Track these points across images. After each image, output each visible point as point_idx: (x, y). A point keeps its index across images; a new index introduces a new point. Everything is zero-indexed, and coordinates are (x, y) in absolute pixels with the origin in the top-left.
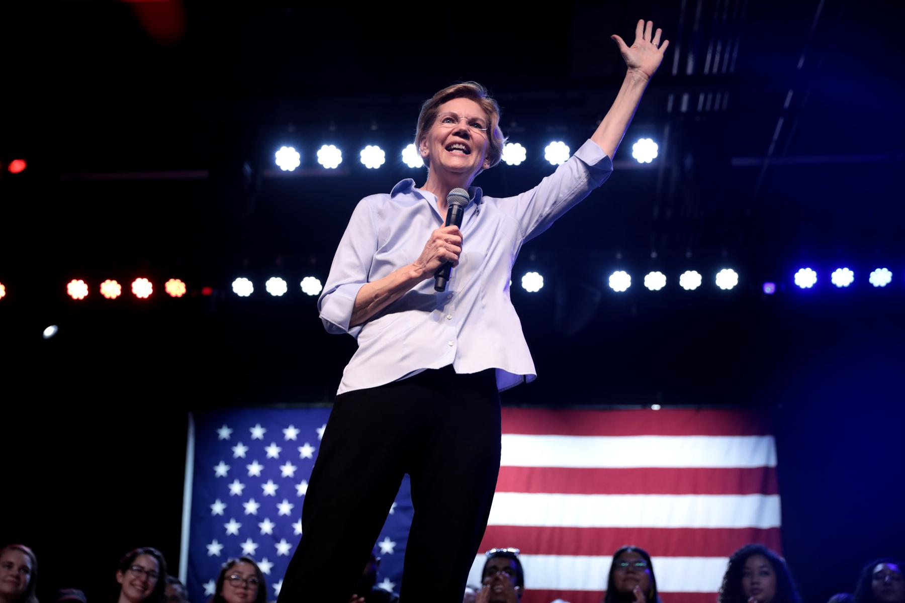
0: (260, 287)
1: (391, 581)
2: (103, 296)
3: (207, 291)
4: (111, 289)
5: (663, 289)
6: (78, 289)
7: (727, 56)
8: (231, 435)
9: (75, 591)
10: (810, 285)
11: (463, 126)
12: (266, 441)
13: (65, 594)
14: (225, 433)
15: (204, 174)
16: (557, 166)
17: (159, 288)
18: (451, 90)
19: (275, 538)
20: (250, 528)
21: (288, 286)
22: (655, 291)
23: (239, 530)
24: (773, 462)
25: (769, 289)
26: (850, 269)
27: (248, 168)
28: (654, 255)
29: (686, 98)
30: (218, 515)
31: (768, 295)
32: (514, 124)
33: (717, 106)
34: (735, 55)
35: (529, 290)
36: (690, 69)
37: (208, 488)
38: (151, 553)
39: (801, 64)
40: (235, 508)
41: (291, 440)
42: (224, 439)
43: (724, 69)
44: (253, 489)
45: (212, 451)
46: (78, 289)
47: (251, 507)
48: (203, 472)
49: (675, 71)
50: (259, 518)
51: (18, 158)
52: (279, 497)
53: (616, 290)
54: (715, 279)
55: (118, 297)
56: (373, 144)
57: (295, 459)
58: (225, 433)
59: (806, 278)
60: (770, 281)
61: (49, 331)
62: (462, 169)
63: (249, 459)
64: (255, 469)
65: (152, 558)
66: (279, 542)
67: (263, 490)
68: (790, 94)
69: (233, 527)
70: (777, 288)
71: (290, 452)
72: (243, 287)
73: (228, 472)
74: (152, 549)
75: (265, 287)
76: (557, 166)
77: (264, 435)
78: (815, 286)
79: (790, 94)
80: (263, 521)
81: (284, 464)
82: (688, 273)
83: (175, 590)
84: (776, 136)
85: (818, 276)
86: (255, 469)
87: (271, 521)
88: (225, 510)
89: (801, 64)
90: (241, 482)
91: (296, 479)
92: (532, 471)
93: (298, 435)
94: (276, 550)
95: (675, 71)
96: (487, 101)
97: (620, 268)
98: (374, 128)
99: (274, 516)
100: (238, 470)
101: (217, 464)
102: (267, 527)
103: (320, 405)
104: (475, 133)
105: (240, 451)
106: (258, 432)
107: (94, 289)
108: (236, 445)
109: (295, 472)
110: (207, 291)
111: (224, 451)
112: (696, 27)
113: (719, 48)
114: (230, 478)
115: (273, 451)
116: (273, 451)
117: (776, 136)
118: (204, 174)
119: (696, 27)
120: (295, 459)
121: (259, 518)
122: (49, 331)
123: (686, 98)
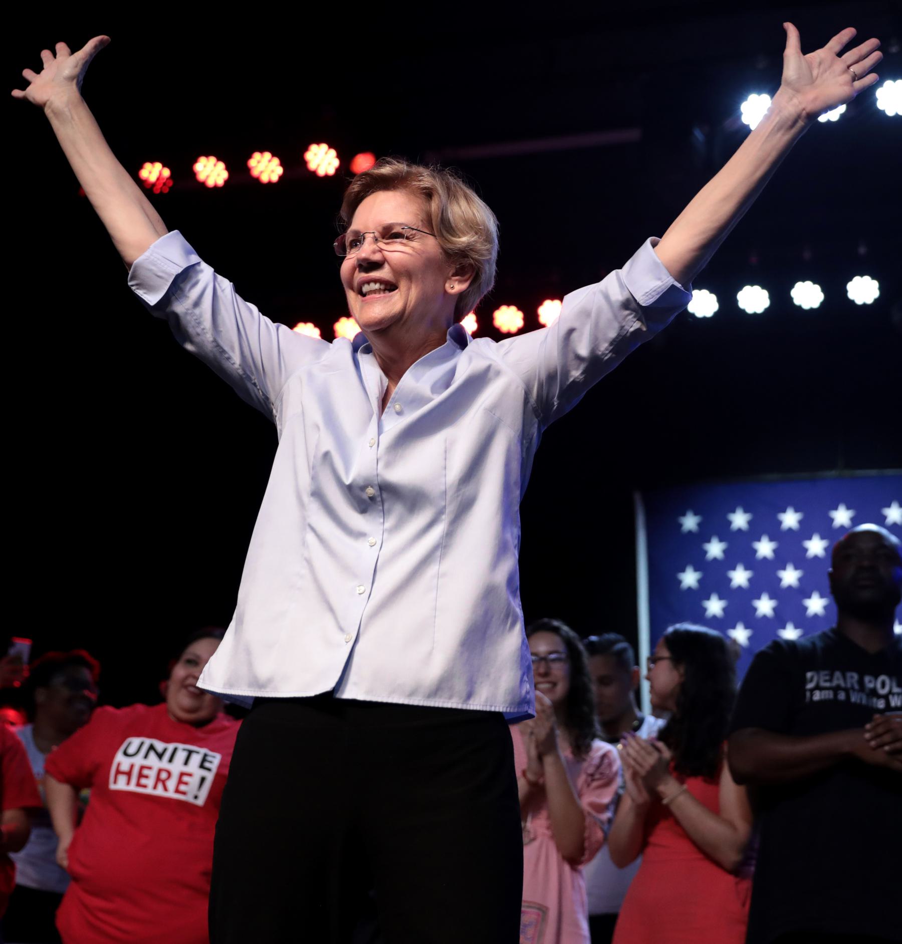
8: (700, 525)
11: (366, 250)
12: (754, 533)
14: (690, 522)
15: (633, 135)
16: (543, 326)
27: (699, 135)
38: (556, 630)
41: (790, 530)
45: (674, 551)
48: (664, 583)
57: (800, 560)
63: (730, 561)
65: (556, 639)
67: (755, 609)
71: (790, 548)
73: (700, 581)
74: (556, 623)
75: (823, 290)
76: (543, 326)
81: (784, 569)
90: (721, 598)
91: (803, 591)
93: (800, 522)
96: (426, 178)
100: (715, 579)
101: (683, 570)
103: (833, 473)
104: (398, 253)
105: (715, 549)
106: (790, 519)
109: (800, 580)
111: (690, 550)
115: (765, 548)
118: (633, 135)
120: (800, 560)
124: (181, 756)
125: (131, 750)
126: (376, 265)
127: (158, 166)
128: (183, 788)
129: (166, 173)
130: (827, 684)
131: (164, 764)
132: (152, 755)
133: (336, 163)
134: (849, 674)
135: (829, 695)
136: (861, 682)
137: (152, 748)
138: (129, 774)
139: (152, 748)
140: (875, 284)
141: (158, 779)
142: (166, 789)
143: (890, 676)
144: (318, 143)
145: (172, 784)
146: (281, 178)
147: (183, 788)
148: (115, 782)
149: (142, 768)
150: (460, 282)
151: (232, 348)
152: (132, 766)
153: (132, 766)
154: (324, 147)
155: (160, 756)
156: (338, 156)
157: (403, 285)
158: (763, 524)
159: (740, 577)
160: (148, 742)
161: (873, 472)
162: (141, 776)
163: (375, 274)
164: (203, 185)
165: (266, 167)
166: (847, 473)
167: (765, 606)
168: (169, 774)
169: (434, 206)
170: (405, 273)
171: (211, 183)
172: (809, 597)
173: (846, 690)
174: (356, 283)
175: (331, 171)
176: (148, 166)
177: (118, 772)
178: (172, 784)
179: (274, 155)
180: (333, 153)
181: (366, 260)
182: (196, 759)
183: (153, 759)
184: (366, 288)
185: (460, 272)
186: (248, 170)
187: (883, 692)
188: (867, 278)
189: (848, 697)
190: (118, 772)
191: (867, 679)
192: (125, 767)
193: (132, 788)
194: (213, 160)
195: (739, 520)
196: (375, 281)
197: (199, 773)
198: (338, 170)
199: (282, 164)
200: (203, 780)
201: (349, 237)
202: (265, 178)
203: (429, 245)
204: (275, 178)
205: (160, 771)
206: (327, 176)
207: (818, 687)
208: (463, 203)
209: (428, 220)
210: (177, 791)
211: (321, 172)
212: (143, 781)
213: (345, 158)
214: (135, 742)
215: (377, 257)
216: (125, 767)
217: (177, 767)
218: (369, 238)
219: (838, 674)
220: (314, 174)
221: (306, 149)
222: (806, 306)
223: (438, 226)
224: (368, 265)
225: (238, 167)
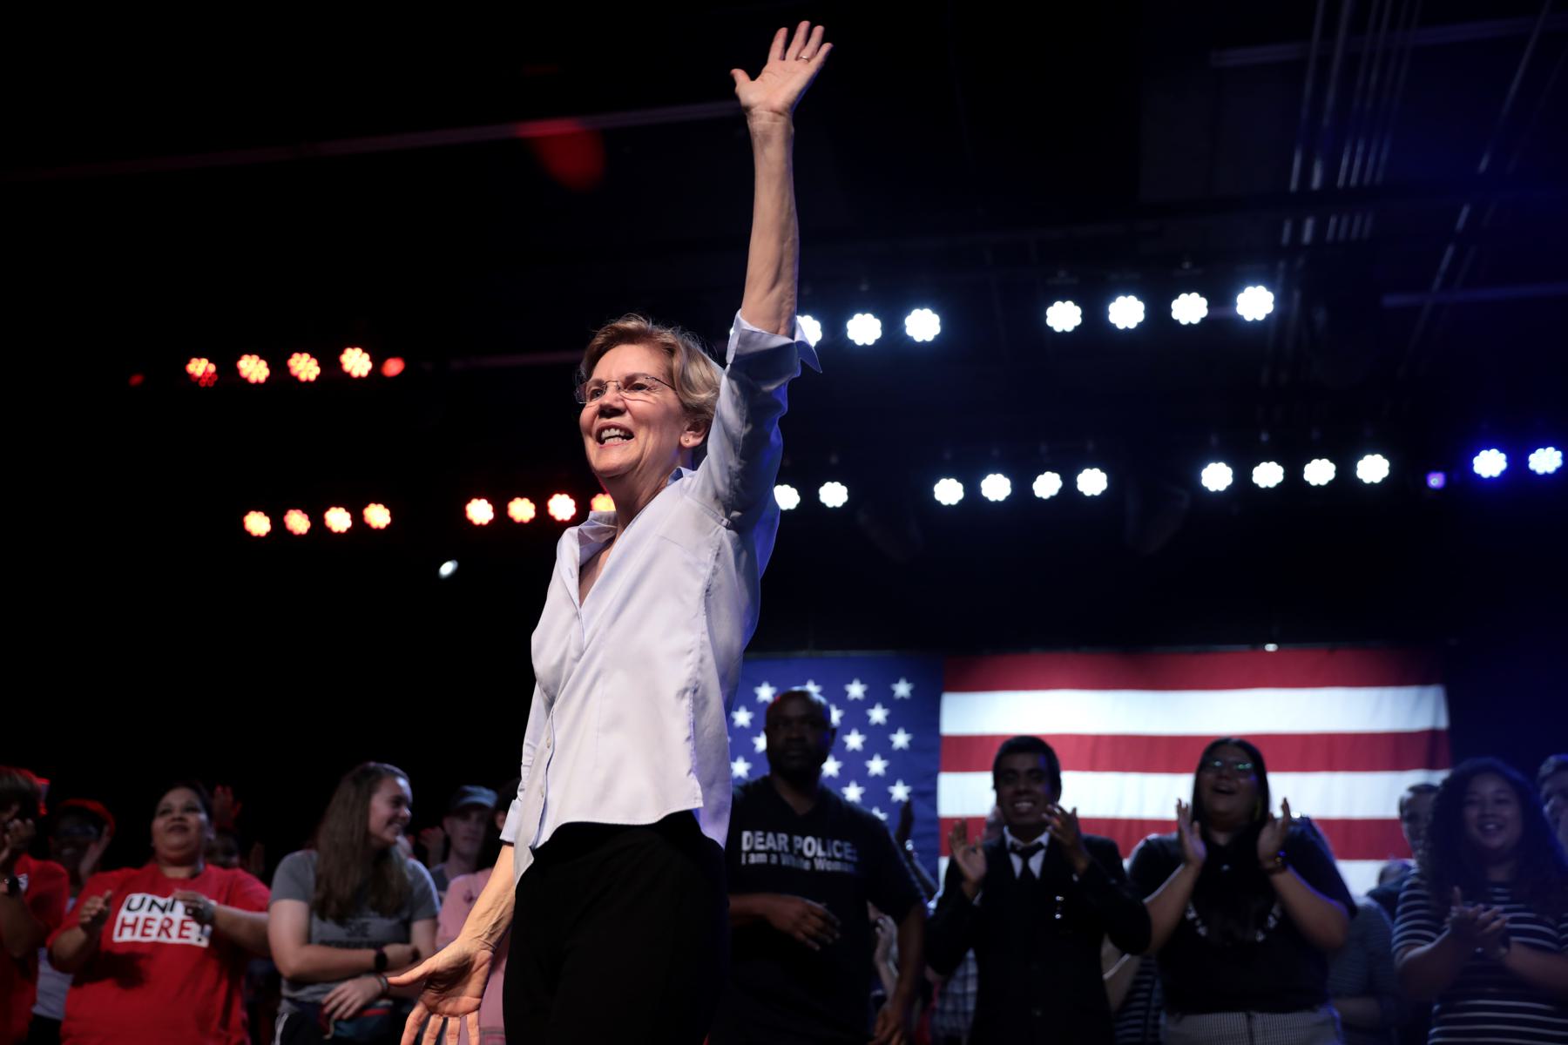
0: (972, 490)
5: (961, 502)
6: (480, 511)
7: (1371, 160)
10: (954, 502)
11: (609, 397)
18: (599, 340)
21: (818, 495)
24: (1443, 723)
25: (1435, 481)
26: (1501, 451)
28: (1264, 437)
29: (1309, 224)
31: (1435, 490)
32: (1062, 274)
33: (1354, 234)
34: (1384, 157)
35: (830, 505)
36: (1316, 182)
39: (1483, 165)
43: (1367, 180)
46: (480, 511)
49: (1294, 185)
51: (393, 355)
52: (867, 753)
53: (945, 502)
54: (1200, 478)
56: (864, 312)
58: (902, 689)
59: (1490, 463)
60: (1436, 470)
61: (447, 569)
62: (617, 469)
68: (1465, 211)
70: (1448, 480)
78: (1504, 474)
79: (1465, 211)
82: (1368, 458)
84: (1444, 265)
85: (980, 489)
89: (1483, 165)
92: (1098, 741)
95: (1294, 185)
96: (668, 336)
97: (1217, 459)
98: (864, 288)
99: (862, 778)
103: (803, 653)
104: (638, 402)
107: (972, 490)
112: (1326, 122)
113: (1360, 149)
117: (1444, 265)
119: (1326, 122)
122: (447, 569)
123: (1309, 224)
125: (135, 905)
126: (618, 412)
127: (204, 362)
128: (185, 933)
129: (212, 368)
130: (761, 847)
132: (155, 908)
133: (369, 366)
134: (780, 836)
135: (762, 858)
136: (791, 844)
137: (153, 903)
138: (134, 926)
139: (153, 903)
140: (844, 490)
142: (169, 936)
143: (816, 837)
144: (353, 347)
145: (174, 931)
147: (185, 933)
148: (120, 934)
149: (147, 919)
155: (163, 910)
156: (371, 360)
157: (641, 434)
160: (149, 898)
161: (838, 653)
162: (145, 926)
163: (615, 420)
164: (246, 380)
165: (305, 367)
167: (878, 715)
168: (171, 922)
169: (676, 363)
170: (643, 421)
171: (253, 379)
173: (778, 853)
174: (595, 430)
175: (364, 373)
176: (194, 361)
177: (123, 925)
178: (174, 931)
181: (609, 406)
183: (156, 912)
184: (606, 434)
186: (288, 369)
187: (809, 854)
189: (779, 860)
191: (797, 838)
193: (137, 937)
194: (255, 358)
195: (856, 690)
196: (616, 427)
199: (319, 365)
201: (591, 386)
202: (303, 377)
204: (312, 377)
206: (360, 378)
207: (753, 851)
208: (702, 365)
209: (670, 374)
210: (180, 936)
211: (355, 374)
212: (148, 931)
213: (378, 361)
214: (136, 899)
215: (619, 405)
218: (612, 387)
219: (770, 836)
220: (348, 375)
221: (342, 352)
223: (676, 381)
224: (607, 412)
225: (330, 363)
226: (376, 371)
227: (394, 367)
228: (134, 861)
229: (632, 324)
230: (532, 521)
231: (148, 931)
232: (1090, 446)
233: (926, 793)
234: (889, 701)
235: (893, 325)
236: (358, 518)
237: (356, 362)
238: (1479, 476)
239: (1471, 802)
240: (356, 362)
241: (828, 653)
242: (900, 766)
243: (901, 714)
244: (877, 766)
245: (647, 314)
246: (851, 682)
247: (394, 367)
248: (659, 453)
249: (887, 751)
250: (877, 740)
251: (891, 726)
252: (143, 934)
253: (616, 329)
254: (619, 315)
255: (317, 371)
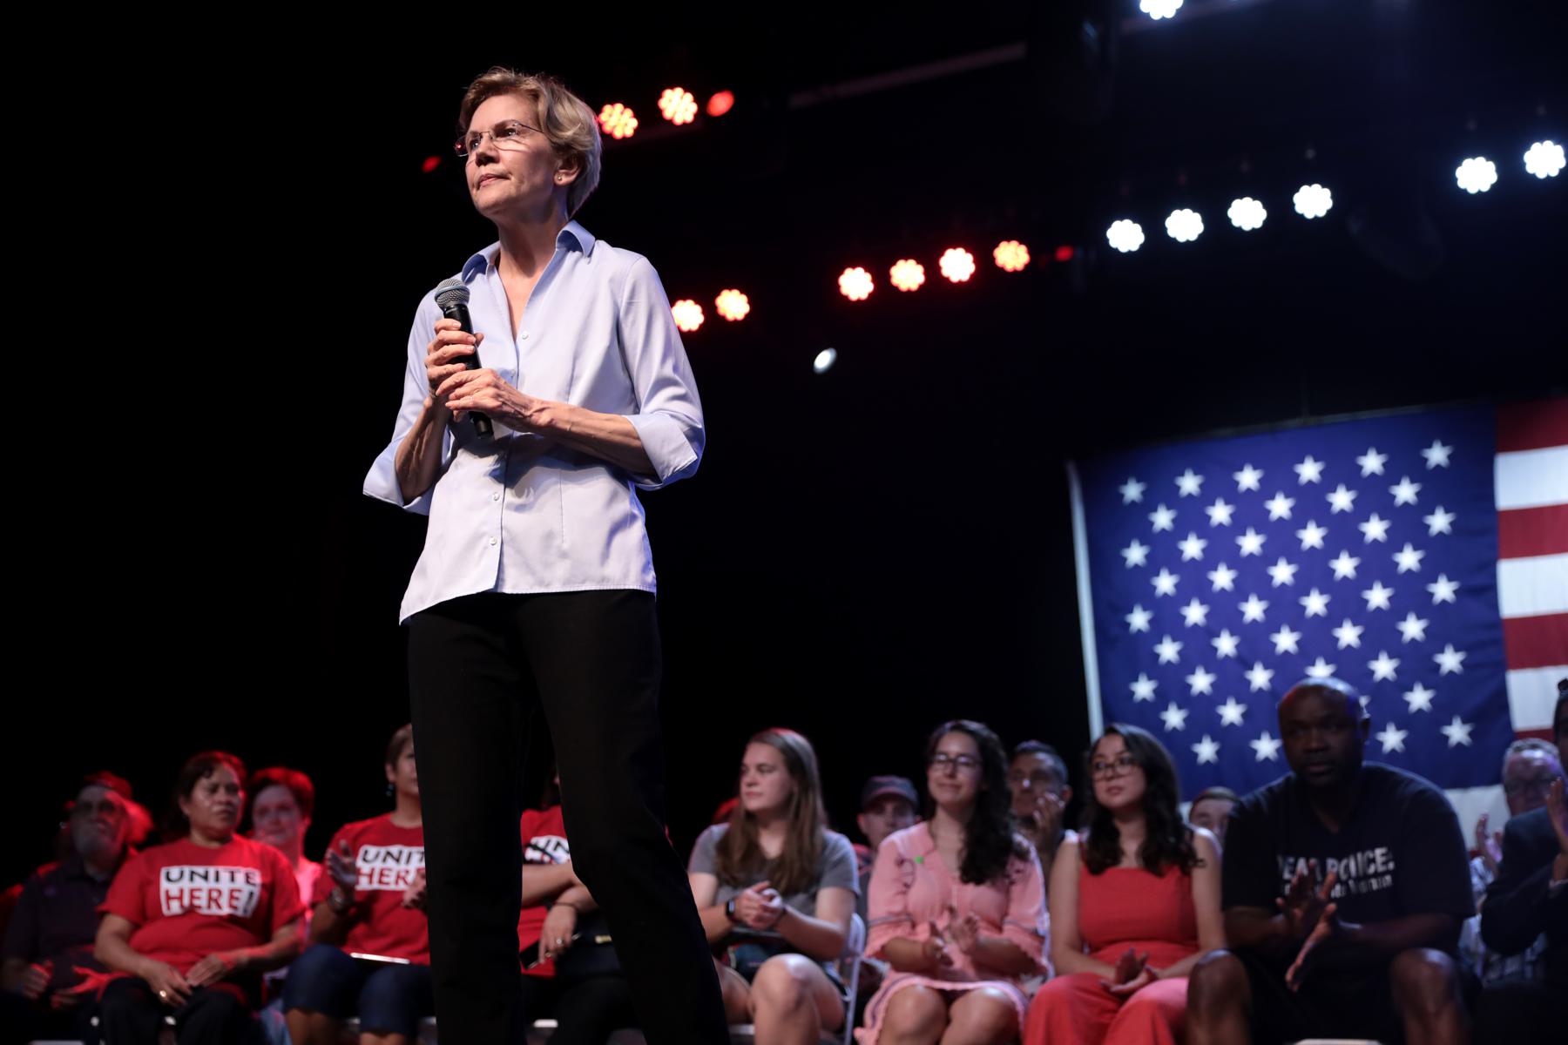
1: (1464, 722)
2: (896, 289)
3: (1064, 254)
4: (908, 275)
6: (856, 284)
8: (1144, 493)
9: (898, 781)
10: (1193, 237)
13: (881, 785)
14: (1133, 491)
15: (1017, 51)
17: (985, 260)
18: (471, 95)
19: (1244, 661)
20: (1198, 647)
21: (1205, 221)
22: (1240, 229)
23: (1180, 653)
27: (1090, 31)
30: (1139, 631)
37: (1119, 586)
40: (1167, 618)
41: (1190, 496)
42: (1133, 502)
44: (1194, 581)
45: (1116, 525)
47: (1195, 613)
50: (1209, 631)
52: (1210, 561)
55: (921, 287)
58: (1437, 455)
61: (824, 360)
63: (1180, 531)
64: (1192, 548)
66: (1251, 668)
69: (1168, 651)
72: (1125, 236)
73: (1147, 557)
77: (1201, 486)
80: (1218, 636)
83: (1041, 761)
86: (1192, 548)
87: (1232, 634)
88: (1150, 622)
94: (1249, 683)
96: (531, 83)
100: (1164, 552)
101: (1128, 546)
102: (1226, 644)
103: (1292, 423)
106: (1248, 478)
108: (1155, 510)
110: (1064, 254)
111: (1135, 523)
114: (1152, 567)
116: (1251, 543)
118: (1017, 51)
121: (1209, 631)
122: (824, 360)
124: (225, 876)
131: (212, 884)
132: (196, 878)
133: (694, 108)
137: (192, 873)
140: (1197, 217)
141: (210, 898)
142: (219, 907)
146: (636, 130)
147: (235, 903)
149: (192, 891)
150: (567, 174)
151: (635, 348)
152: (182, 891)
153: (182, 891)
154: (679, 91)
155: (206, 877)
156: (696, 100)
158: (1279, 479)
159: (1254, 609)
161: (1343, 417)
162: (382, 875)
166: (1313, 421)
168: (220, 892)
172: (1275, 564)
175: (689, 118)
177: (169, 898)
178: (224, 901)
179: (626, 106)
180: (689, 97)
182: (240, 877)
185: (567, 165)
188: (1317, 187)
190: (169, 898)
192: (174, 892)
193: (375, 886)
197: (247, 889)
198: (696, 116)
199: (636, 116)
200: (251, 894)
201: (469, 138)
203: (538, 140)
204: (629, 132)
205: (210, 891)
206: (685, 124)
211: (678, 120)
213: (702, 100)
216: (174, 892)
217: (225, 885)
218: (486, 136)
222: (1009, 267)
226: (702, 113)
227: (721, 103)
228: (170, 834)
229: (497, 77)
230: (1027, 266)
231: (385, 879)
232: (1541, 111)
233: (1481, 589)
234: (1419, 471)
235: (1280, 207)
236: (932, 270)
237: (678, 106)
238: (750, 302)
239: (1097, 767)
240: (678, 106)
241: (1329, 419)
242: (1439, 556)
243: (1436, 489)
244: (1408, 559)
245: (508, 65)
246: (1365, 454)
247: (721, 103)
248: (534, 190)
249: (1421, 538)
250: (1407, 525)
251: (1425, 504)
252: (380, 882)
253: (484, 83)
254: (486, 70)
255: (634, 123)
